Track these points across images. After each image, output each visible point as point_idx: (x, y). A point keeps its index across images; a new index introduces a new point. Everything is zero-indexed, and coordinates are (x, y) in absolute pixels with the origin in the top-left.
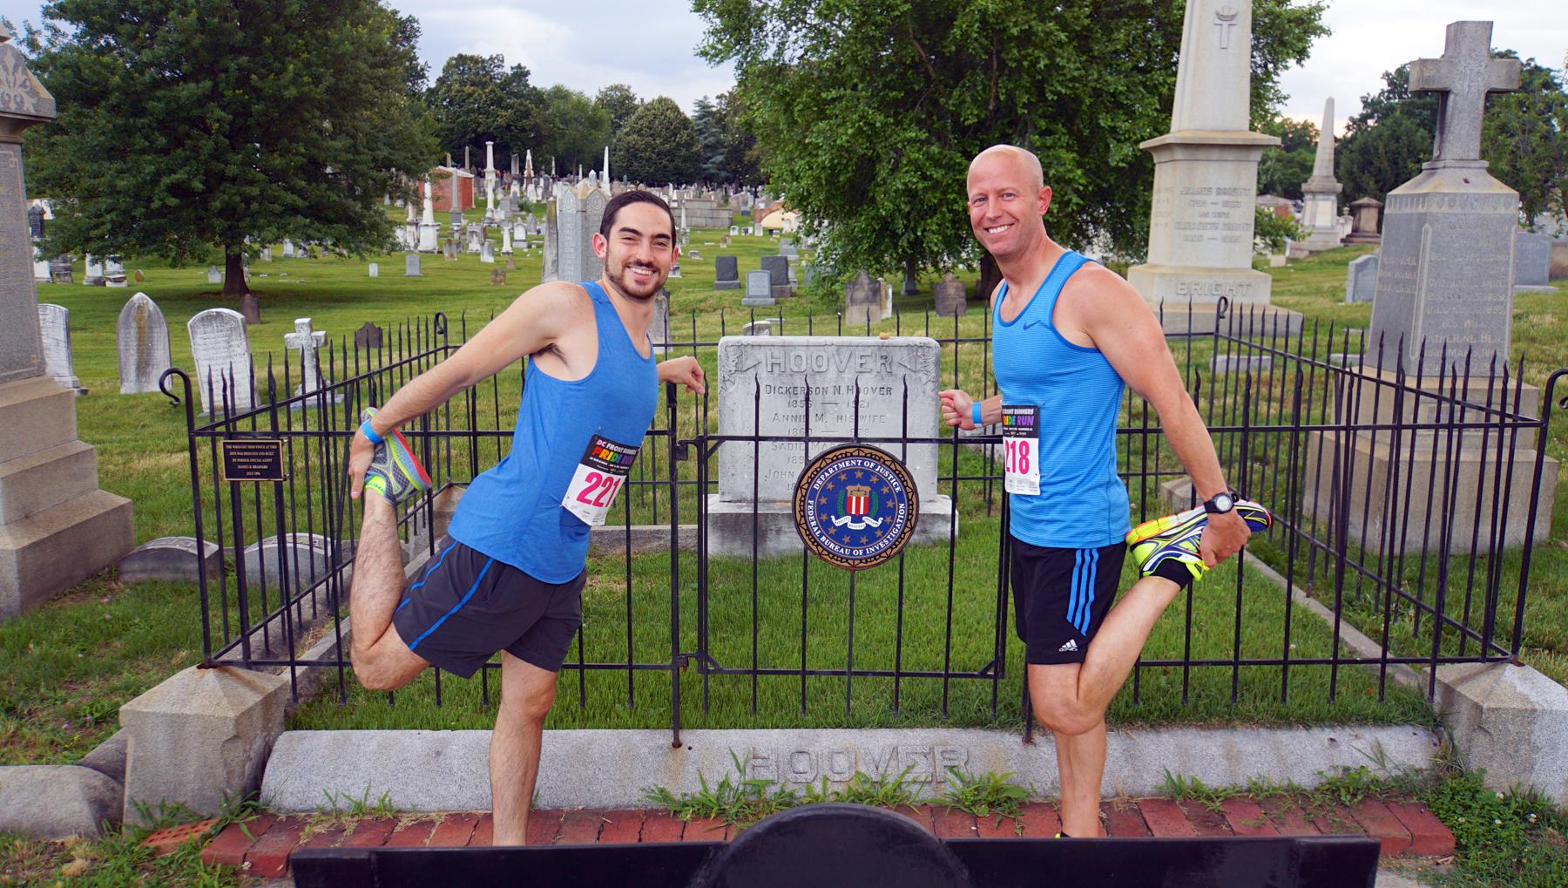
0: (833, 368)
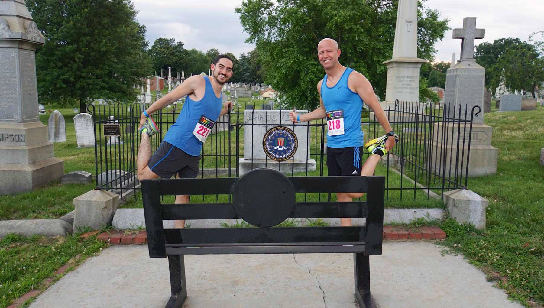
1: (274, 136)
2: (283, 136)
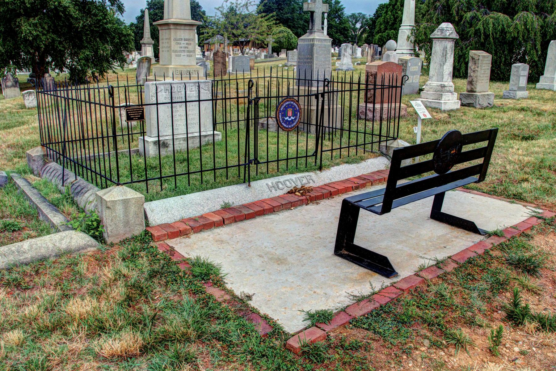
2: (291, 107)
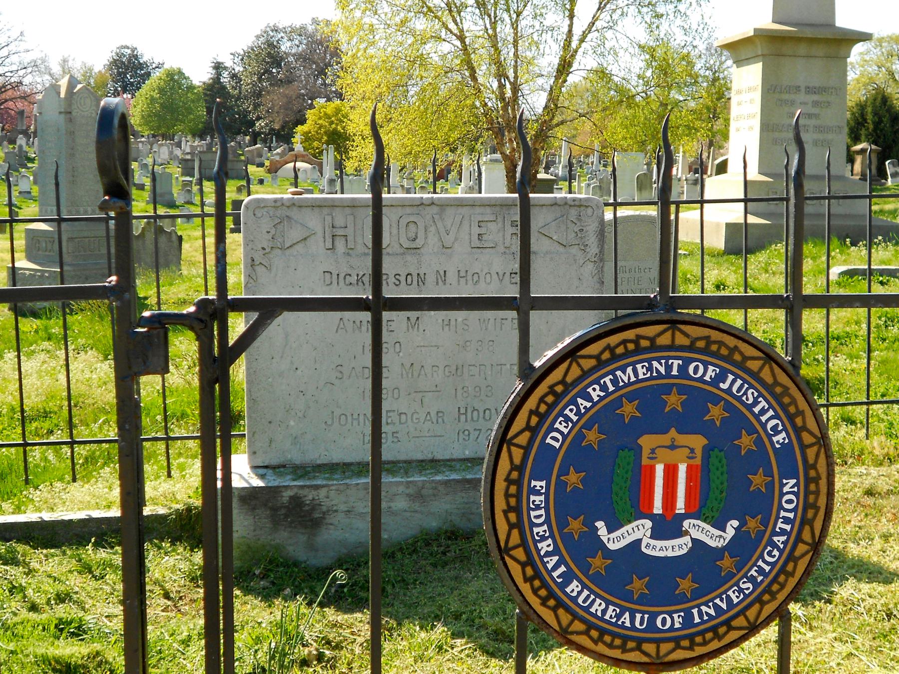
0: (433, 240)
1: (605, 415)
2: (688, 422)
